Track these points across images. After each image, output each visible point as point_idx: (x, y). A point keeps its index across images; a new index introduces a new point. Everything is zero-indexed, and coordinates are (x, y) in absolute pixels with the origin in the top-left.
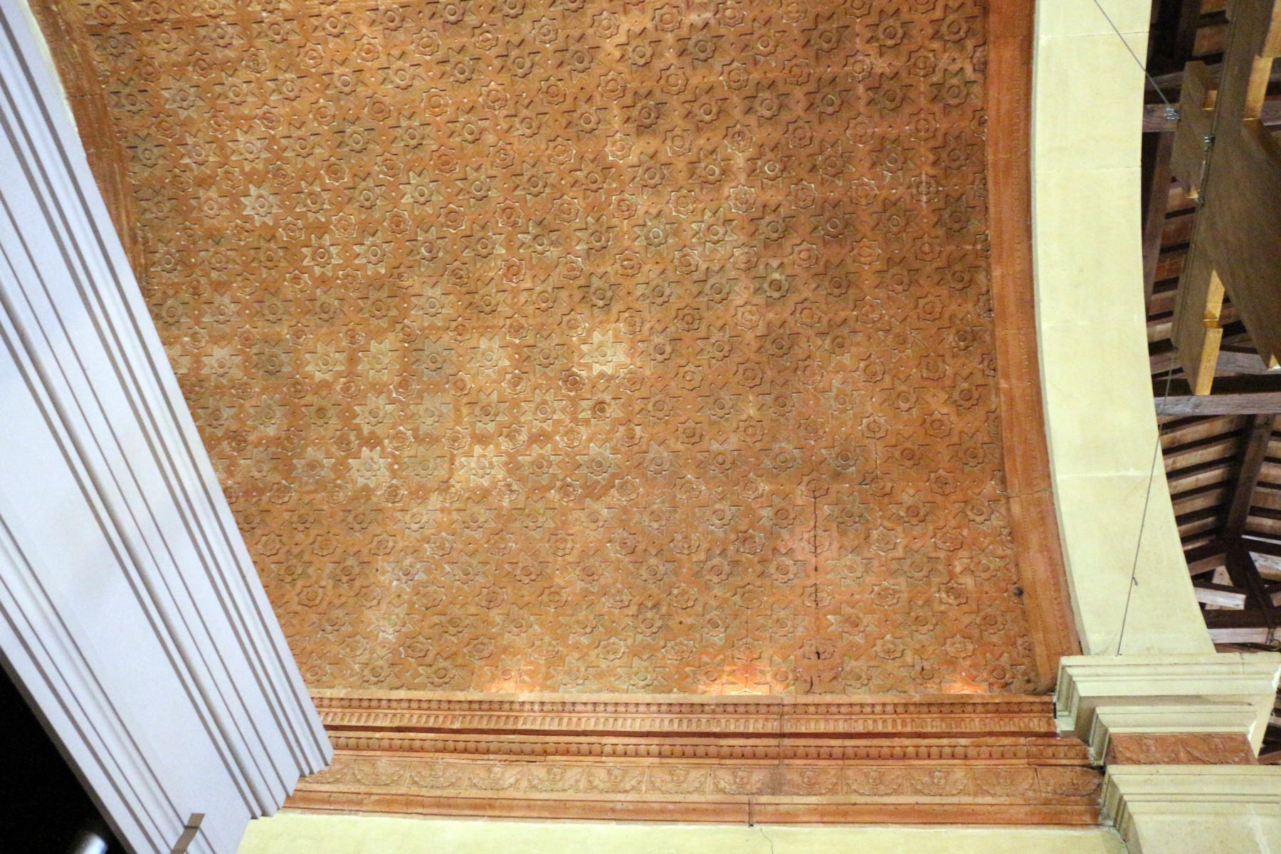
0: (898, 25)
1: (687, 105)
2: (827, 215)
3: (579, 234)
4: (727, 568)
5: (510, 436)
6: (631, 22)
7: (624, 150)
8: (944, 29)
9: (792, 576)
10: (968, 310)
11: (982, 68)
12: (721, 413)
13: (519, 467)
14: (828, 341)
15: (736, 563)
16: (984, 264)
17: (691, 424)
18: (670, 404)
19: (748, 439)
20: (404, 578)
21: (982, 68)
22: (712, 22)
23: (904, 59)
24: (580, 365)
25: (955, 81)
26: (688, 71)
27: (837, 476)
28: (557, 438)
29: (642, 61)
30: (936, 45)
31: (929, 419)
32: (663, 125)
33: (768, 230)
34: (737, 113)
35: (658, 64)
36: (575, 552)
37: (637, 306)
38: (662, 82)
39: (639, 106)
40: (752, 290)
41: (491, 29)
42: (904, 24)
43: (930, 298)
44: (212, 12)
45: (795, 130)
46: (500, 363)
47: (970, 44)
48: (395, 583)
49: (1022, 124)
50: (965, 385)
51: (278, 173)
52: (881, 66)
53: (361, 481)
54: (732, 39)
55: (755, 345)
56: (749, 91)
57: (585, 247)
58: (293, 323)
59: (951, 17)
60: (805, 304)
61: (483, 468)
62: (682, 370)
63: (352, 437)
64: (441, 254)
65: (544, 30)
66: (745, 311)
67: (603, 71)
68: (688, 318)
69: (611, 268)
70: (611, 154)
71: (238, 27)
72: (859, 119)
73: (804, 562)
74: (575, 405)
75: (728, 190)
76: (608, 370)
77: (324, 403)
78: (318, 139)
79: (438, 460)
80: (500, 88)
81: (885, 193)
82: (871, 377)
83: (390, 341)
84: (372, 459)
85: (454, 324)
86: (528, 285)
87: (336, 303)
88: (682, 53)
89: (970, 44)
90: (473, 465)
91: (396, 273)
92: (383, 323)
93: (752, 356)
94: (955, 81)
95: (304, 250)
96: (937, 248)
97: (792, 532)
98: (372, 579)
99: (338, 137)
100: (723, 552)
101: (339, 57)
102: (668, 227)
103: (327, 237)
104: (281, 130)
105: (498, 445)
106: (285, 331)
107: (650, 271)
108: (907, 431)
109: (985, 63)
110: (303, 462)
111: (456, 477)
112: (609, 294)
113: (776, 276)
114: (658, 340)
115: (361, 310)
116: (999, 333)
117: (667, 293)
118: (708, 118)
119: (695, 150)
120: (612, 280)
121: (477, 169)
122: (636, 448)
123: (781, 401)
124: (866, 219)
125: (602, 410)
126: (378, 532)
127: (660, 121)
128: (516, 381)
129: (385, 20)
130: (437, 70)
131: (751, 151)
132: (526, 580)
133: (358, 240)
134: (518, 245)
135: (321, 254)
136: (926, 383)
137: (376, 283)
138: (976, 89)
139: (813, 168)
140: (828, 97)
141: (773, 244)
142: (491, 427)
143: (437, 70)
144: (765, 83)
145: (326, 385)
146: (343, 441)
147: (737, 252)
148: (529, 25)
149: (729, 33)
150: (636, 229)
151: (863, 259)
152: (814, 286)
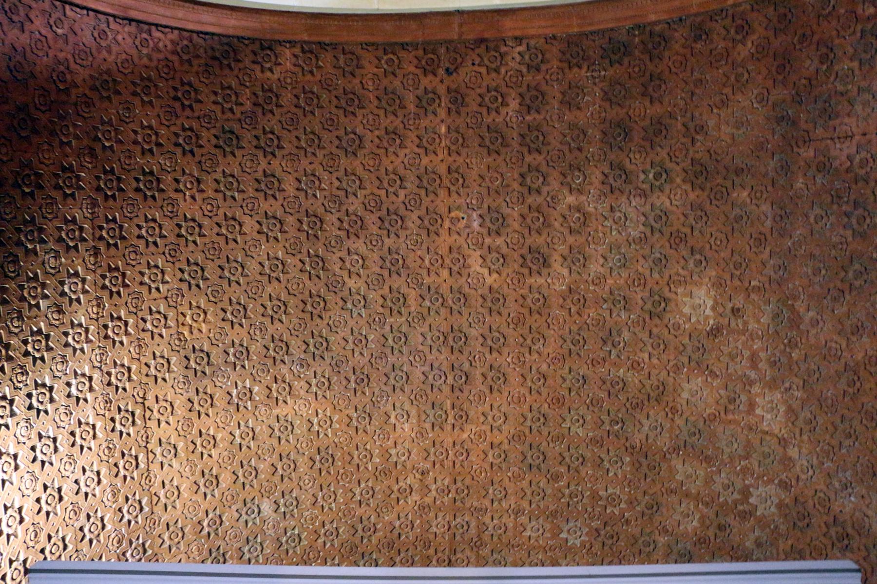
0: (489, 95)
1: (532, 233)
2: (612, 140)
3: (614, 315)
4: (860, 211)
5: (751, 383)
6: (475, 265)
7: (558, 278)
8: (494, 66)
9: (869, 155)
10: (680, 34)
11: (519, 40)
12: (745, 218)
13: (774, 379)
14: (698, 137)
15: (856, 205)
16: (648, 29)
17: (752, 242)
18: (737, 257)
19: (764, 196)
20: (850, 490)
21: (519, 40)
22: (479, 212)
23: (511, 90)
24: (705, 324)
25: (527, 57)
26: (509, 230)
27: (794, 123)
28: (755, 347)
29: (501, 260)
30: (503, 71)
31: (756, 56)
32: (545, 250)
33: (619, 180)
34: (540, 199)
35: (504, 250)
36: (839, 341)
37: (666, 278)
38: (516, 248)
39: (531, 265)
40: (660, 194)
41: (473, 355)
42: (489, 91)
43: (670, 64)
44: (446, 527)
45: (86, 52)
46: (700, 385)
47: (503, 49)
48: (852, 499)
49: (555, 10)
50: (733, 31)
51: (554, 514)
52: (514, 104)
53: (773, 509)
54: (491, 200)
55: (698, 192)
56: (525, 190)
57: (623, 311)
58: (657, 532)
59: (486, 62)
60: (671, 154)
61: (773, 409)
62: (713, 247)
63: (740, 508)
64: (620, 415)
65: (476, 321)
66: (674, 199)
67: (506, 286)
68: (677, 241)
69: (638, 296)
70: (560, 287)
71: (457, 514)
72: (548, 118)
73: (859, 146)
74: (733, 331)
75: (591, 209)
76: (710, 303)
77: (715, 524)
78: (534, 483)
79: (764, 443)
80: (511, 355)
81: (598, 101)
82: (724, 103)
83: (677, 463)
84: (758, 496)
85: (670, 415)
86: (646, 356)
87: (646, 497)
88: (498, 234)
89: (503, 49)
90: (769, 416)
91: (631, 450)
92: (664, 466)
93: (706, 194)
94: (527, 57)
95: (608, 511)
96: (637, 62)
97: (835, 158)
98: (848, 517)
99: (534, 469)
100: (847, 215)
101: (482, 456)
102: (613, 252)
103: (600, 493)
104: (525, 504)
105: (757, 395)
106: (662, 540)
107: (643, 267)
108: (764, 72)
109: (516, 38)
110: (755, 552)
111: (776, 431)
112: (657, 297)
113: (651, 176)
114: (691, 265)
115: (653, 480)
116: (695, 10)
117: (658, 255)
118: (541, 219)
119: (562, 229)
120: (648, 294)
121: (564, 380)
122: (767, 286)
123: (739, 172)
124: (616, 113)
125: (738, 310)
126: (812, 504)
127: (542, 251)
128: (713, 374)
129: (461, 421)
130: (496, 394)
131: (566, 191)
132: (858, 384)
133: (605, 471)
134: (618, 360)
135: (612, 500)
136: (730, 61)
137: (637, 466)
138: (532, 43)
139: (580, 149)
140: (533, 139)
141: (627, 177)
142: (744, 398)
143: (496, 394)
144: (520, 180)
145: (702, 519)
146: (744, 516)
147: (634, 204)
148: (471, 329)
149: (488, 201)
150: (613, 275)
151: (642, 114)
152: (659, 149)
